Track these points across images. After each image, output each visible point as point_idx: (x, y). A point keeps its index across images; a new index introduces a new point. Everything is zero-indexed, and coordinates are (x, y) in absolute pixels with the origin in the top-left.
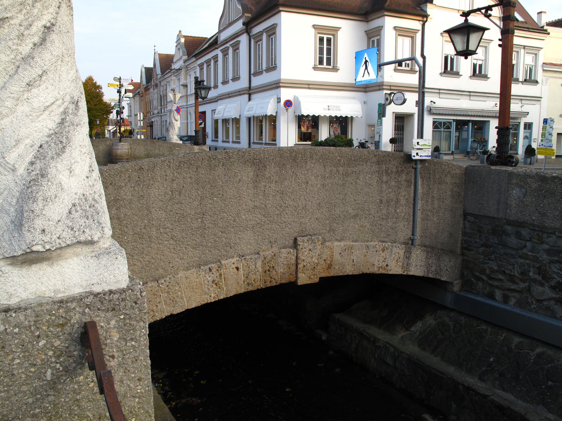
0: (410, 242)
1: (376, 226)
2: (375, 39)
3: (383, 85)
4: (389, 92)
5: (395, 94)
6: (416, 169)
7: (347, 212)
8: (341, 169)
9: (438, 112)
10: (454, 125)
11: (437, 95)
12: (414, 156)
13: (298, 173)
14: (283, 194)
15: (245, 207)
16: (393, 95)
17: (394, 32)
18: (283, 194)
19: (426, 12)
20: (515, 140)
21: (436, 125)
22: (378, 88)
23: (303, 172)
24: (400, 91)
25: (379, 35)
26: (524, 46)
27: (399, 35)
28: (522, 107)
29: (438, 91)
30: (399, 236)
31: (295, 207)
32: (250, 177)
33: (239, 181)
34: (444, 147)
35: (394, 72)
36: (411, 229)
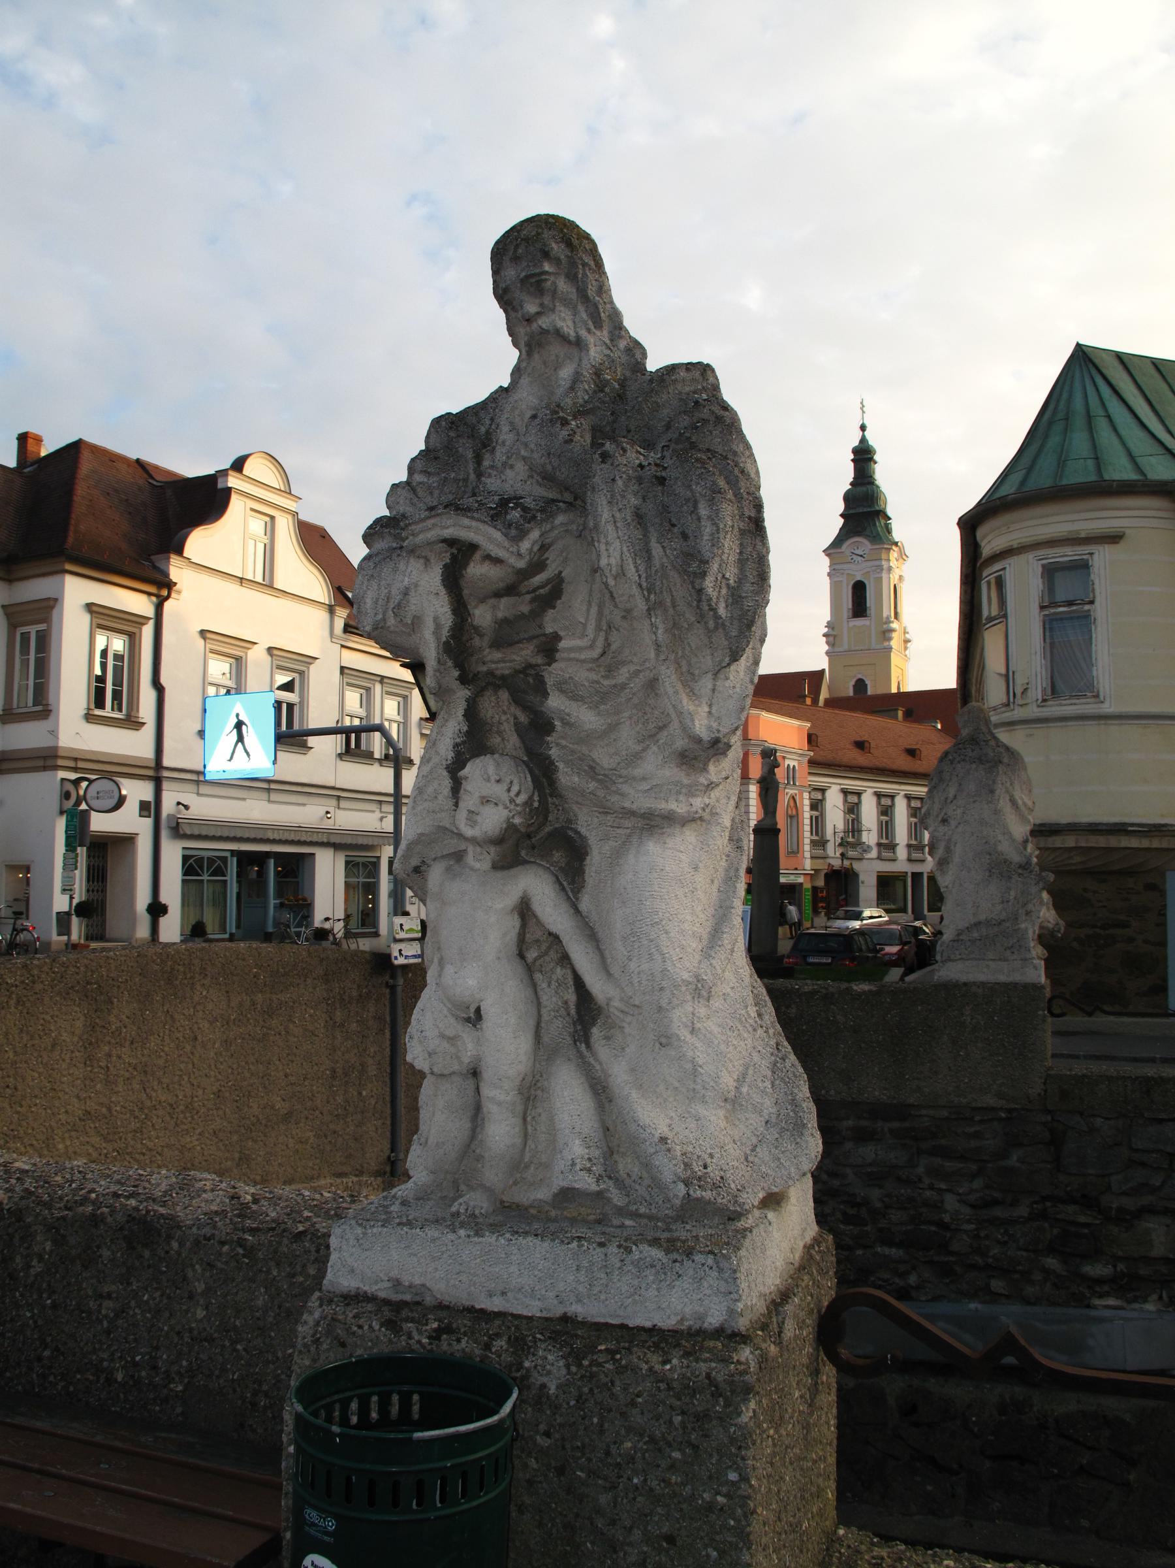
0: (388, 1169)
1: (326, 1136)
2: (33, 630)
3: (56, 757)
4: (73, 776)
5: (91, 781)
6: (393, 989)
7: (273, 1107)
8: (259, 997)
9: (196, 832)
10: (233, 866)
11: (193, 787)
12: (396, 958)
13: (176, 1016)
14: (145, 1072)
15: (63, 1117)
16: (84, 784)
17: (86, 618)
18: (145, 1072)
19: (167, 575)
20: (369, 901)
21: (191, 866)
22: (41, 763)
23: (186, 1012)
24: (108, 776)
25: (47, 619)
26: (383, 677)
27: (100, 626)
28: (381, 819)
29: (265, 786)
30: (368, 1155)
31: (171, 1105)
32: (78, 1032)
33: (53, 1046)
34: (210, 918)
35: (84, 722)
36: (388, 1134)
